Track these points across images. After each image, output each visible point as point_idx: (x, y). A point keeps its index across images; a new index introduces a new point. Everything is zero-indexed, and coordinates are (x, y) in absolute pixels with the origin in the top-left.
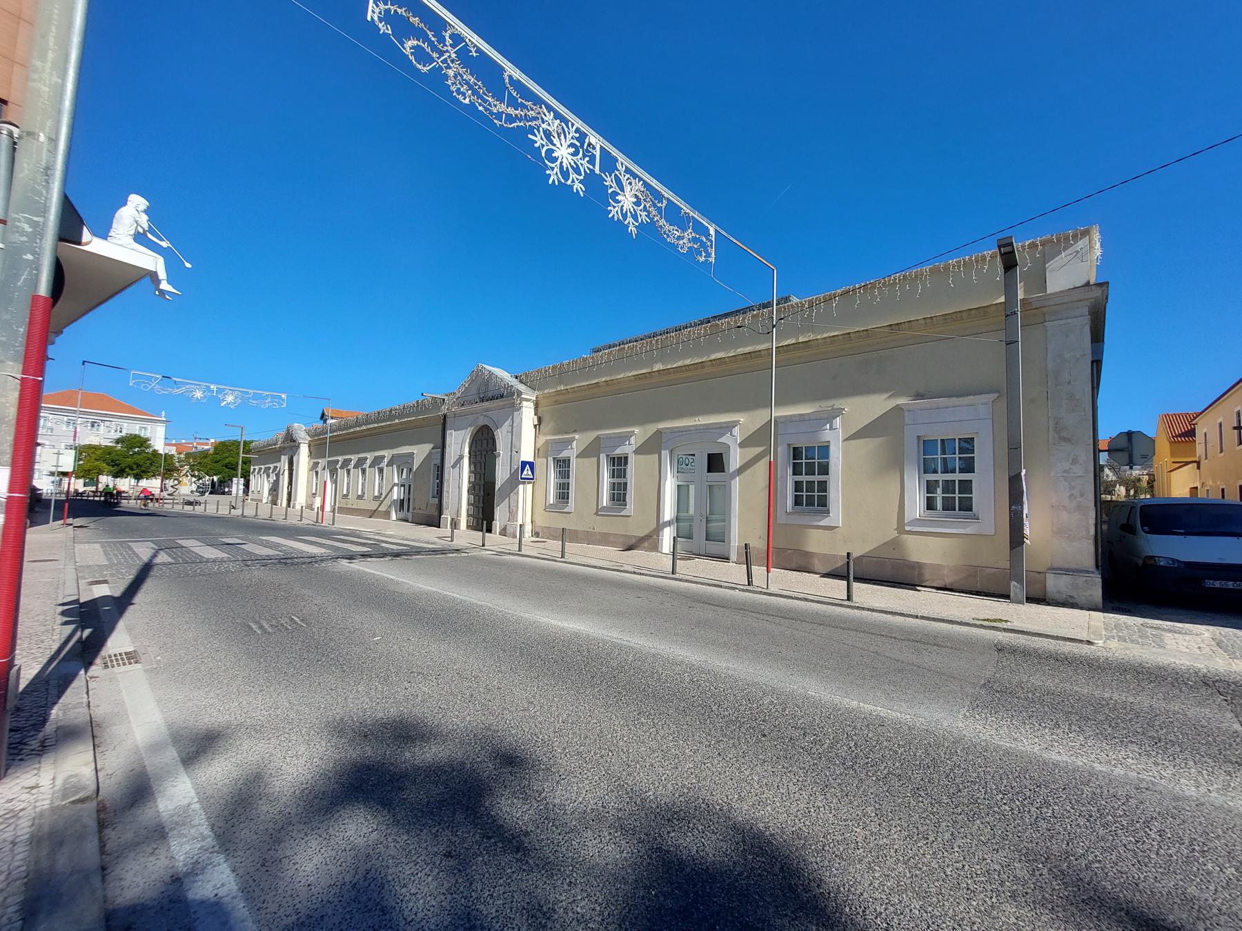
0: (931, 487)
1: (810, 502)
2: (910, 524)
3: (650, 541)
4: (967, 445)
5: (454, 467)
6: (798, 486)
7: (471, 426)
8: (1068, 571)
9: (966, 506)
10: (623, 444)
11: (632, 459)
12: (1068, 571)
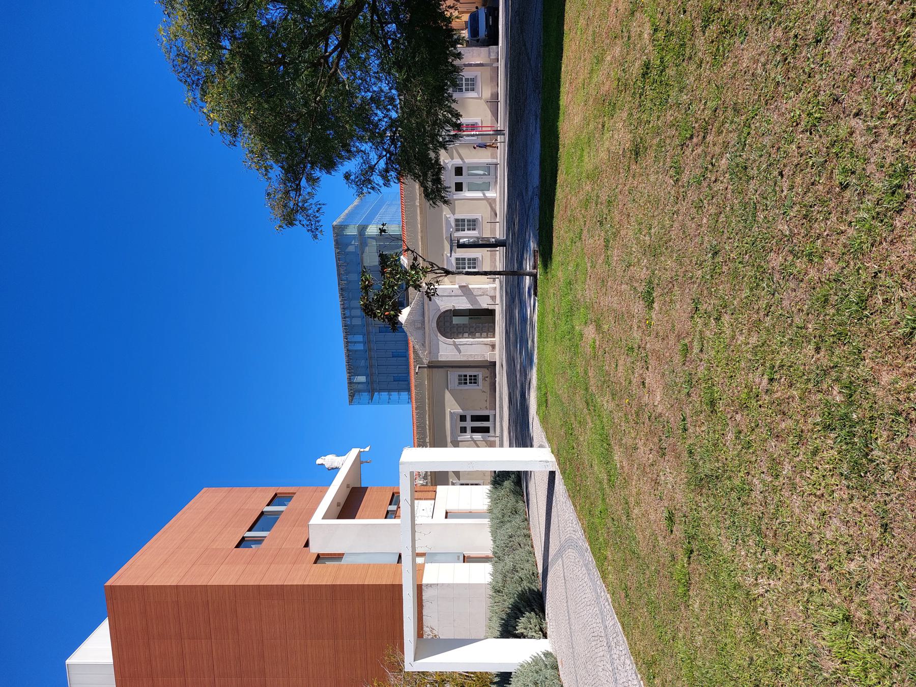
0: (467, 90)
1: (475, 379)
2: (479, 95)
3: (492, 203)
4: (460, 376)
5: (460, 351)
6: (469, 229)
7: (437, 336)
8: (489, 53)
9: (472, 80)
10: (450, 221)
11: (459, 216)
12: (489, 53)
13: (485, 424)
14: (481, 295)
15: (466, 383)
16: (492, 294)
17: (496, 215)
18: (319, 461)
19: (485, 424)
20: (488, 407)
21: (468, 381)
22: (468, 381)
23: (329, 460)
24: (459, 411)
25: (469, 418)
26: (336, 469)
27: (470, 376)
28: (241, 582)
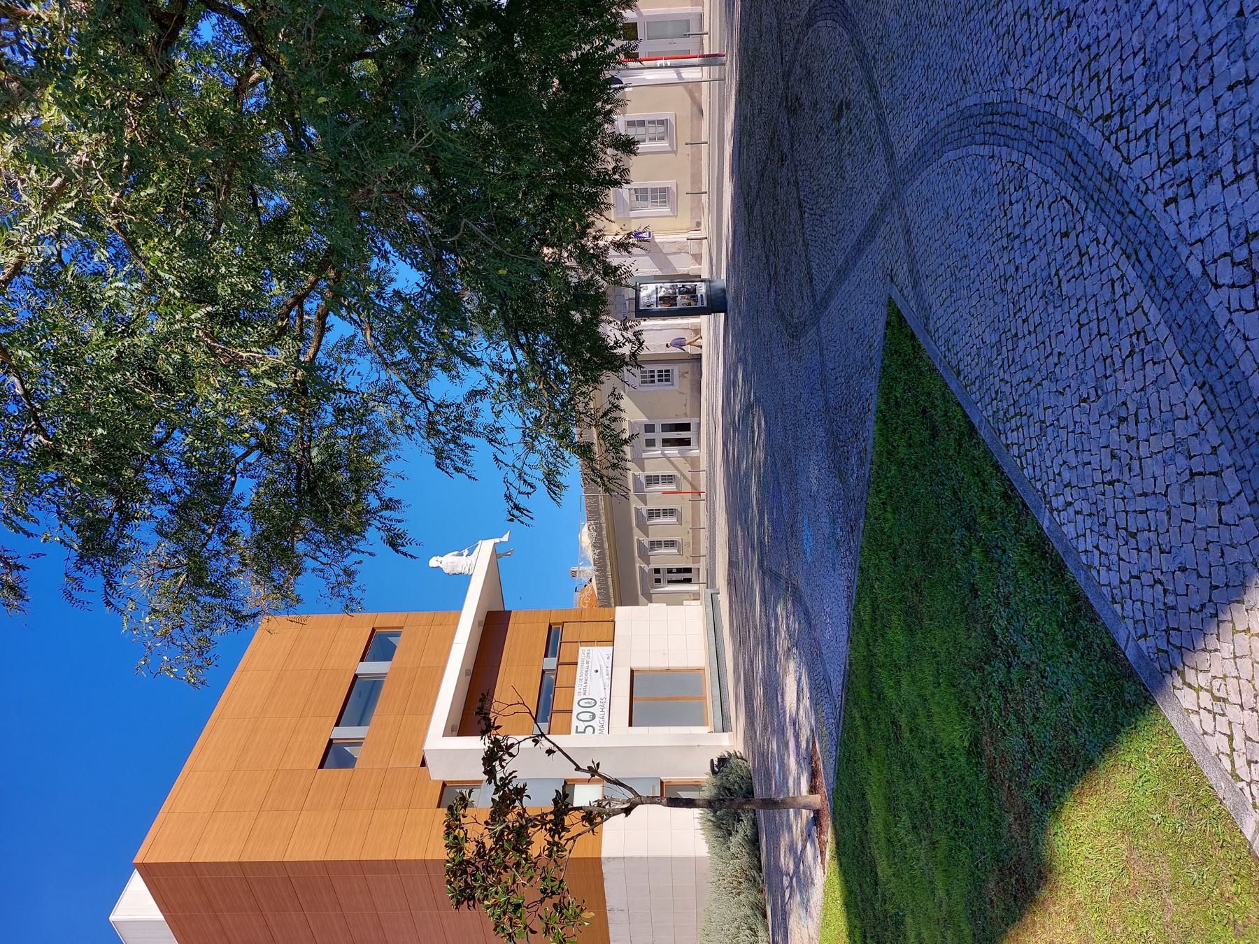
13: (687, 576)
14: (675, 253)
15: (653, 382)
16: (695, 250)
17: (701, 112)
18: (433, 562)
19: (687, 576)
20: (688, 414)
21: (656, 378)
22: (656, 378)
23: (448, 562)
24: (645, 420)
25: (658, 428)
26: (463, 579)
27: (659, 371)
28: (332, 856)
